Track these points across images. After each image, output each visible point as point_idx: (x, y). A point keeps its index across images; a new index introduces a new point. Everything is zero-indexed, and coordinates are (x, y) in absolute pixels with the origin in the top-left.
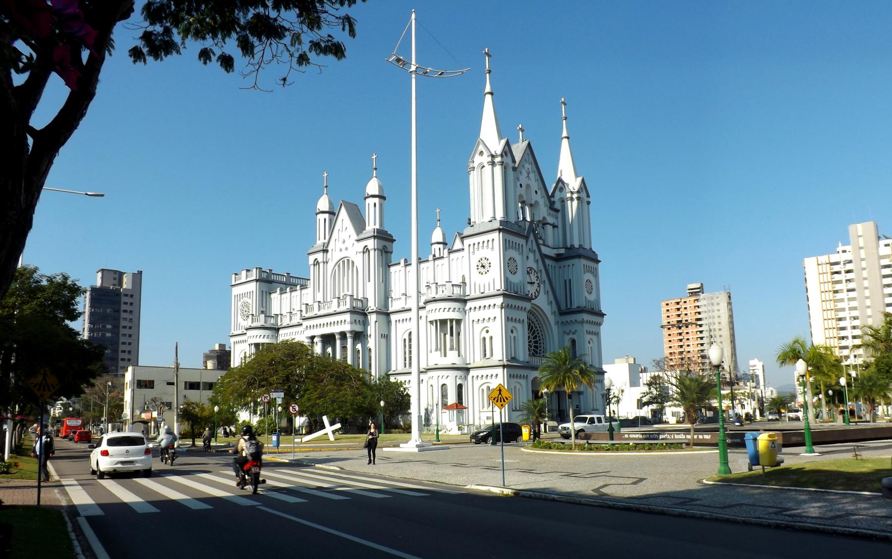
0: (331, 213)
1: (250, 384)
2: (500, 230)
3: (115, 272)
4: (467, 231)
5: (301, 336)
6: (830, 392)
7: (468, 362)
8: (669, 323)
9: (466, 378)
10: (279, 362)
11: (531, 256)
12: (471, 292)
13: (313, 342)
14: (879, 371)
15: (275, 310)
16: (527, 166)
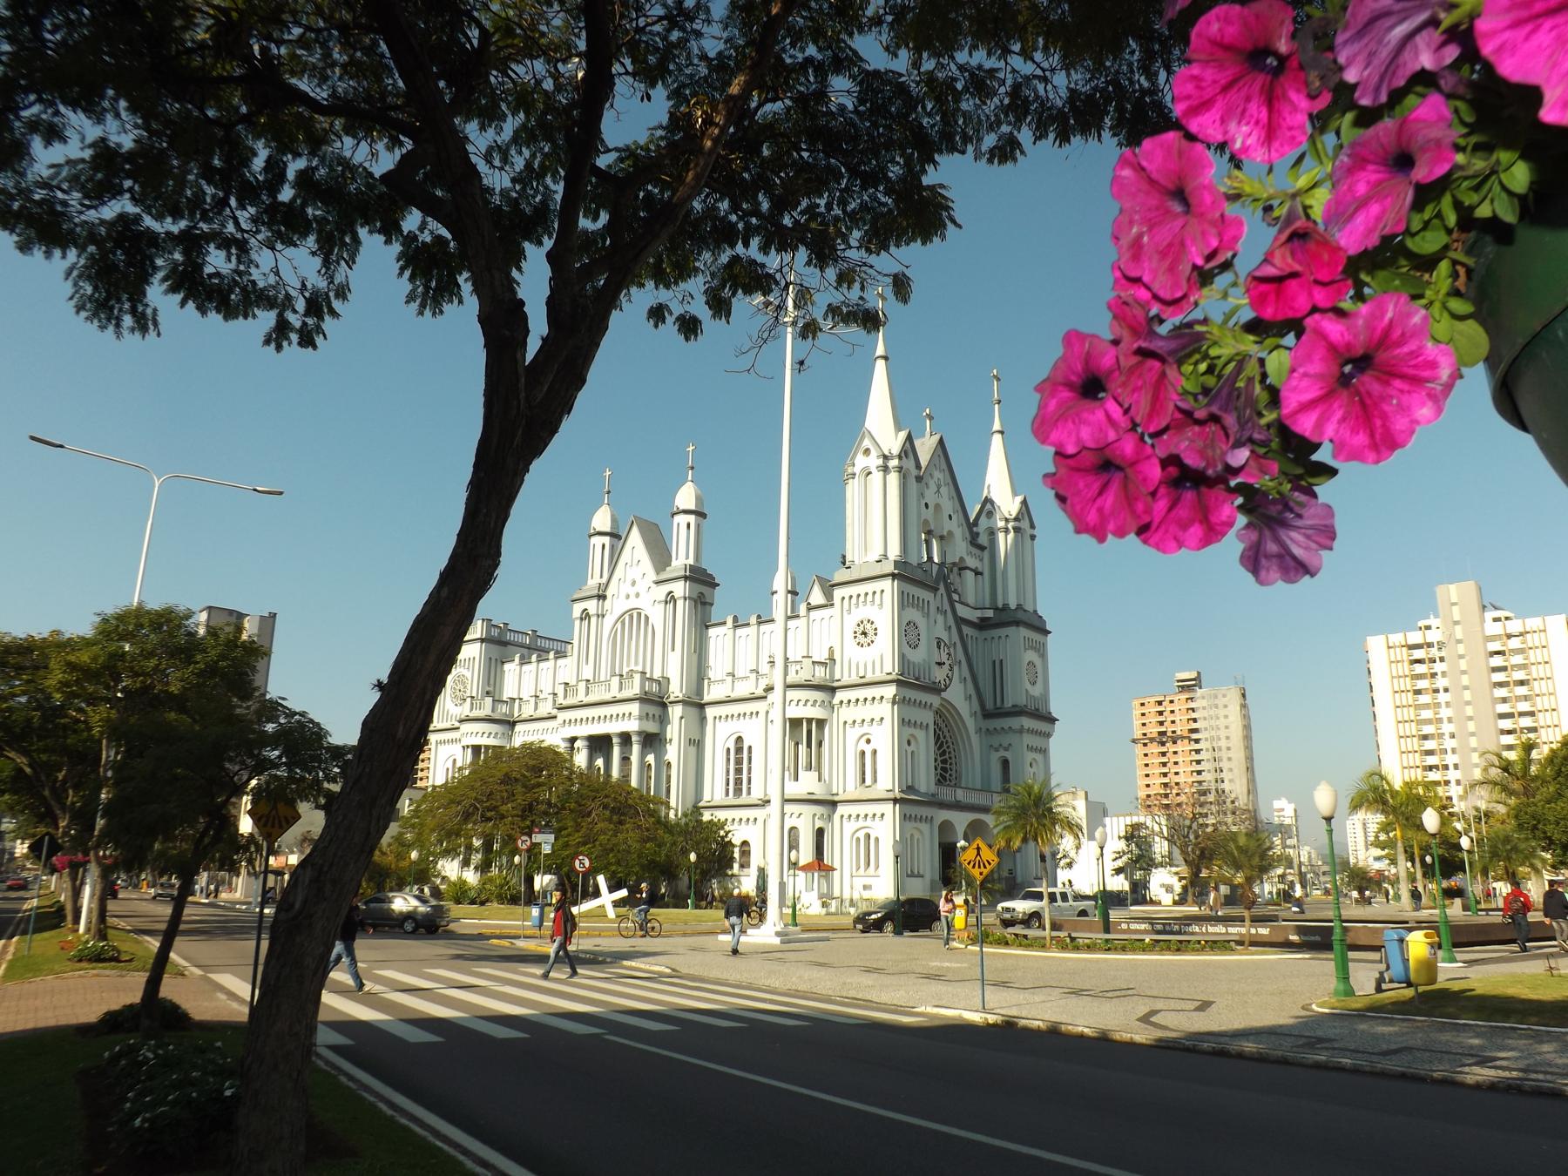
0: (614, 535)
1: (467, 816)
2: (894, 576)
3: (231, 612)
4: (840, 575)
5: (553, 736)
6: (1428, 859)
7: (835, 791)
8: (1145, 734)
9: (830, 818)
10: (516, 780)
11: (940, 618)
12: (843, 675)
13: (572, 748)
14: (1520, 827)
15: (509, 691)
16: (937, 475)
